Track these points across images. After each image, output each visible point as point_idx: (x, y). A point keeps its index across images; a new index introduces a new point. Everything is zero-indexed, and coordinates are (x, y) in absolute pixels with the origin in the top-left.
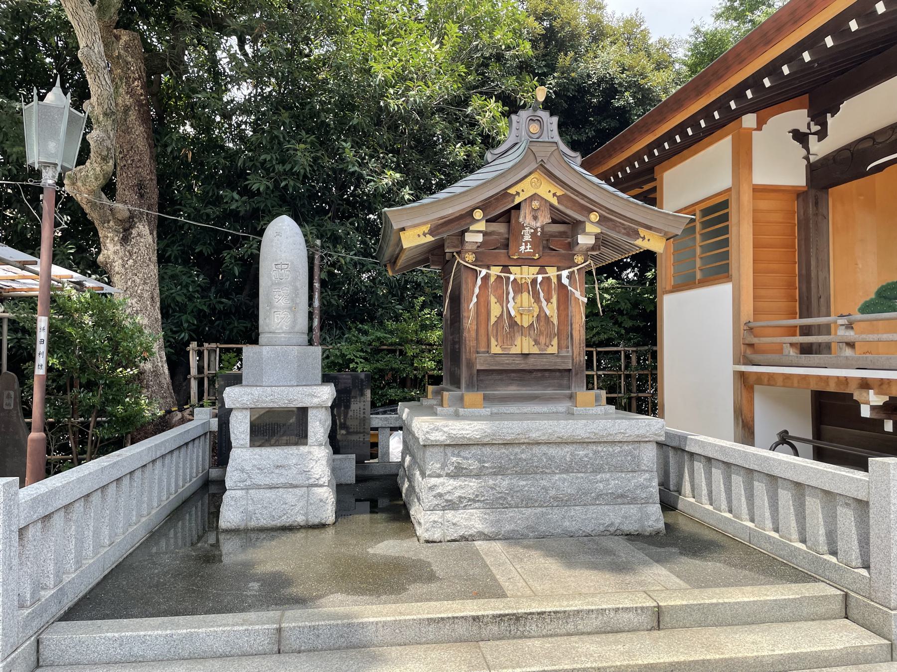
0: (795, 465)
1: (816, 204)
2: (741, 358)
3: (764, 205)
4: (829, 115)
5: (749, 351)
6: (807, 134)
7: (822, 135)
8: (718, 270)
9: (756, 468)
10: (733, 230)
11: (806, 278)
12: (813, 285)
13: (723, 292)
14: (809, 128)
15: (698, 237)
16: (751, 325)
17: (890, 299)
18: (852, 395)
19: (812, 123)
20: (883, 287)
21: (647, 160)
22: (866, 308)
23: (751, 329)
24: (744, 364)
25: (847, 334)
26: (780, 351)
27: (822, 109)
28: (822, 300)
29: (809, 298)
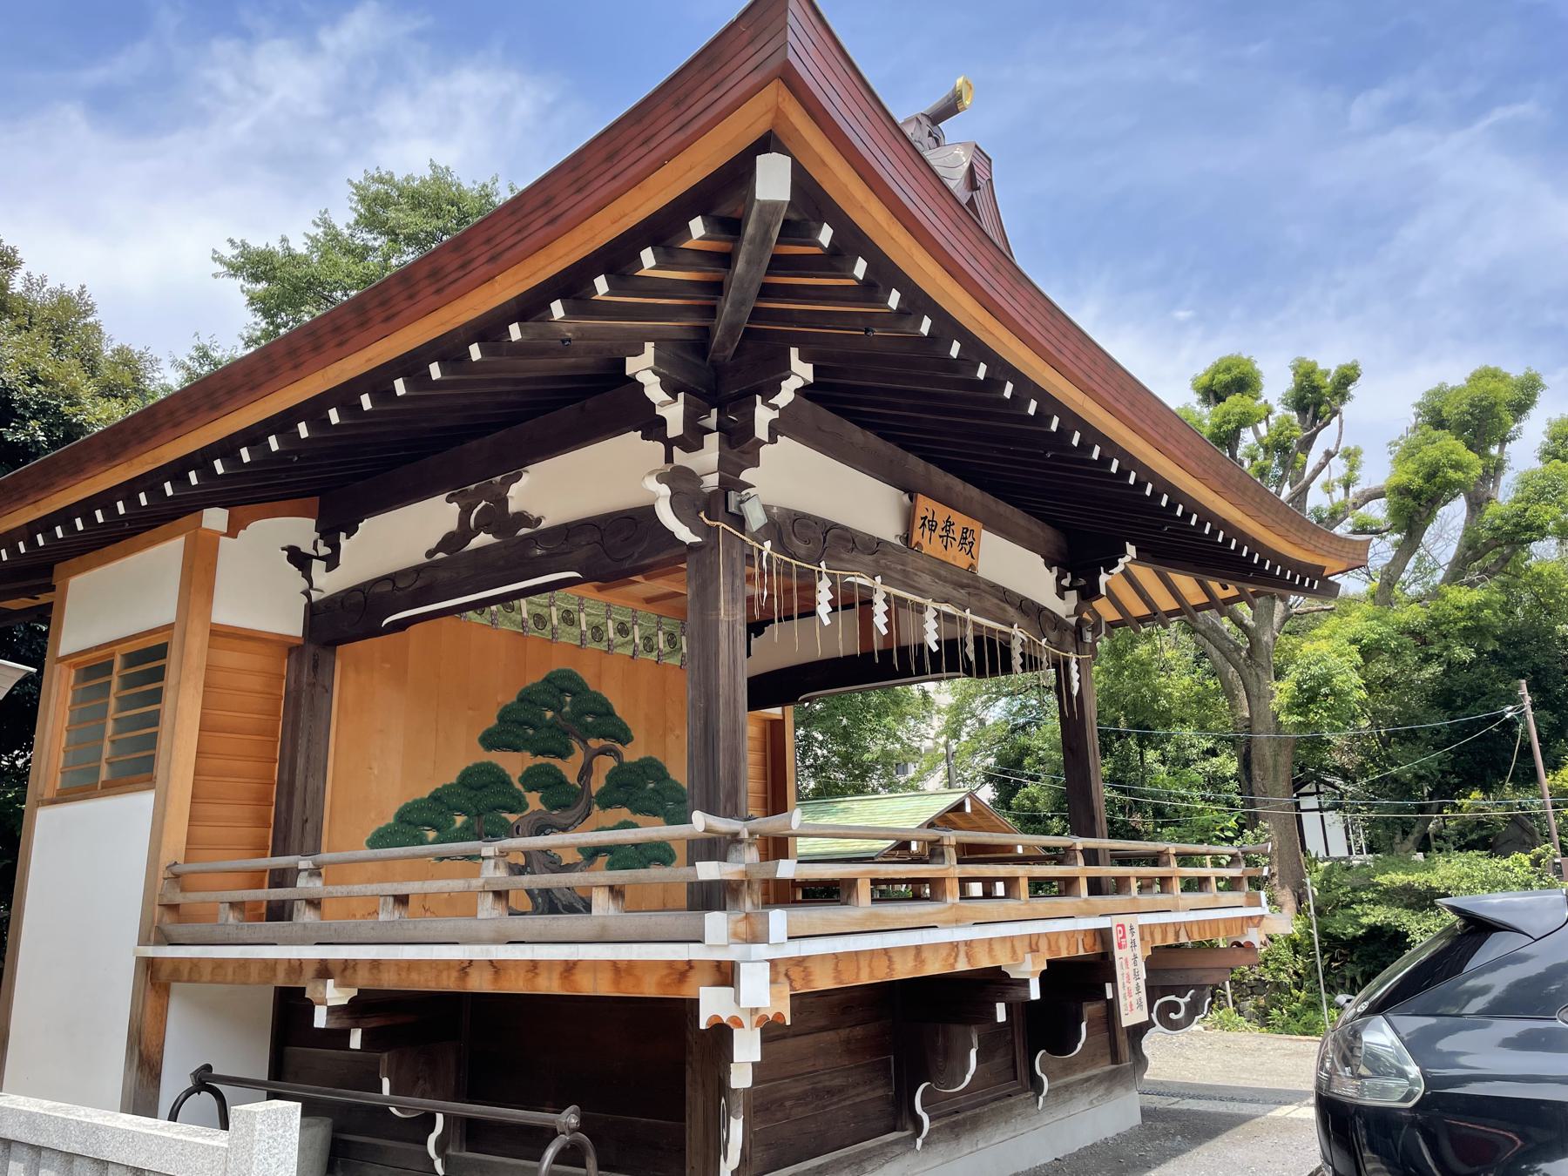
0: (134, 1135)
1: (315, 667)
2: (155, 933)
3: (231, 658)
4: (343, 535)
5: (168, 918)
6: (311, 557)
7: (332, 562)
8: (138, 770)
9: (77, 1149)
10: (168, 696)
11: (287, 789)
12: (297, 801)
13: (142, 803)
14: (315, 548)
15: (113, 702)
16: (176, 869)
17: (416, 826)
18: (304, 989)
19: (320, 542)
20: (407, 805)
21: (23, 550)
22: (380, 839)
23: (177, 876)
24: (158, 943)
25: (311, 885)
26: (213, 917)
27: (336, 524)
28: (309, 826)
29: (288, 822)
